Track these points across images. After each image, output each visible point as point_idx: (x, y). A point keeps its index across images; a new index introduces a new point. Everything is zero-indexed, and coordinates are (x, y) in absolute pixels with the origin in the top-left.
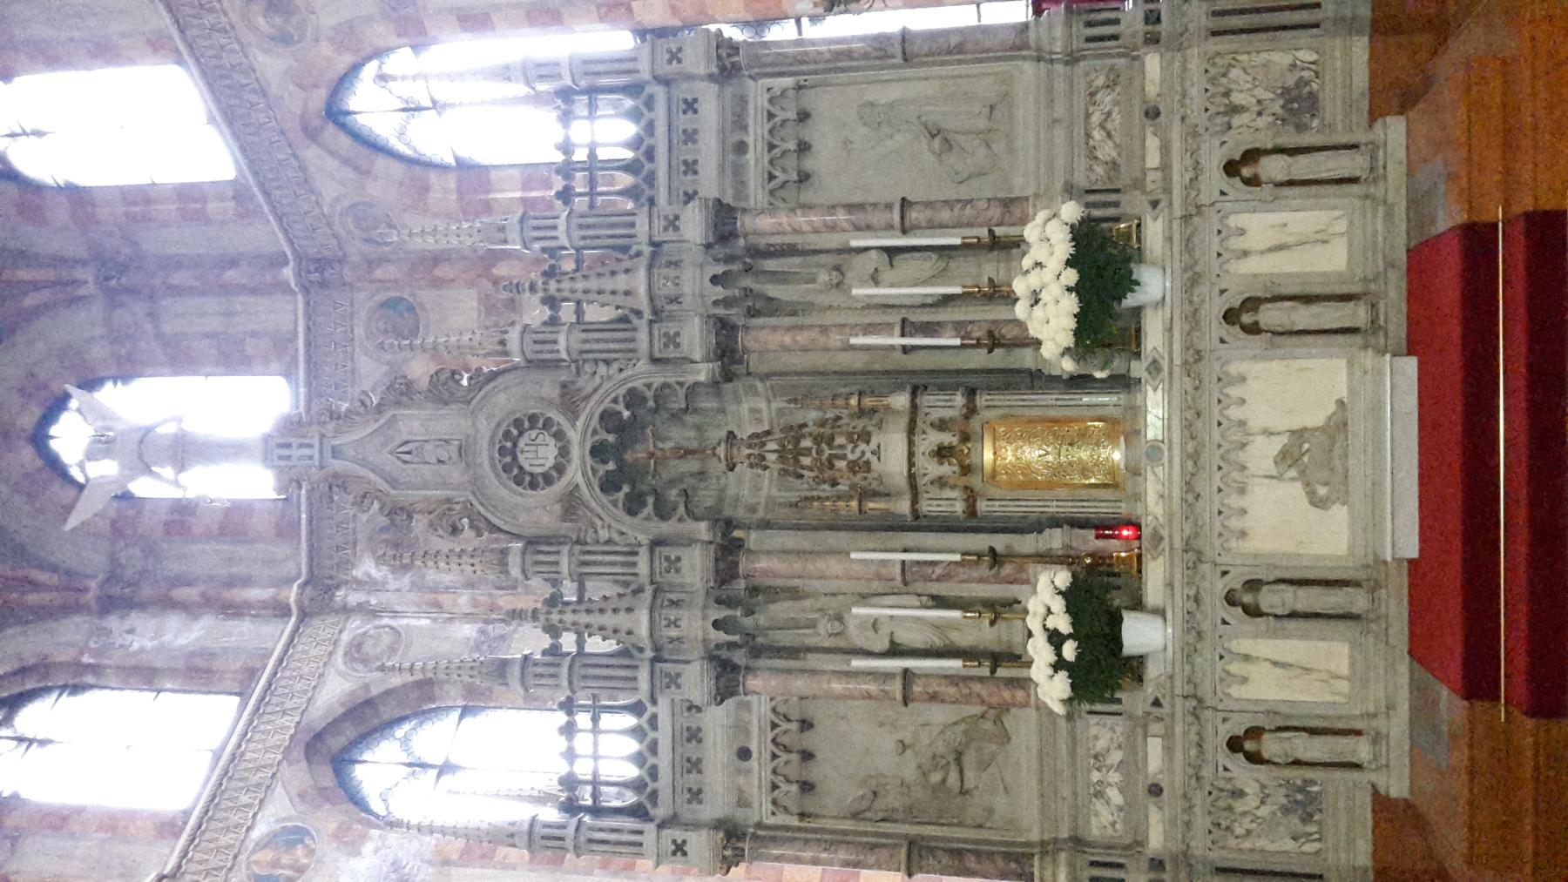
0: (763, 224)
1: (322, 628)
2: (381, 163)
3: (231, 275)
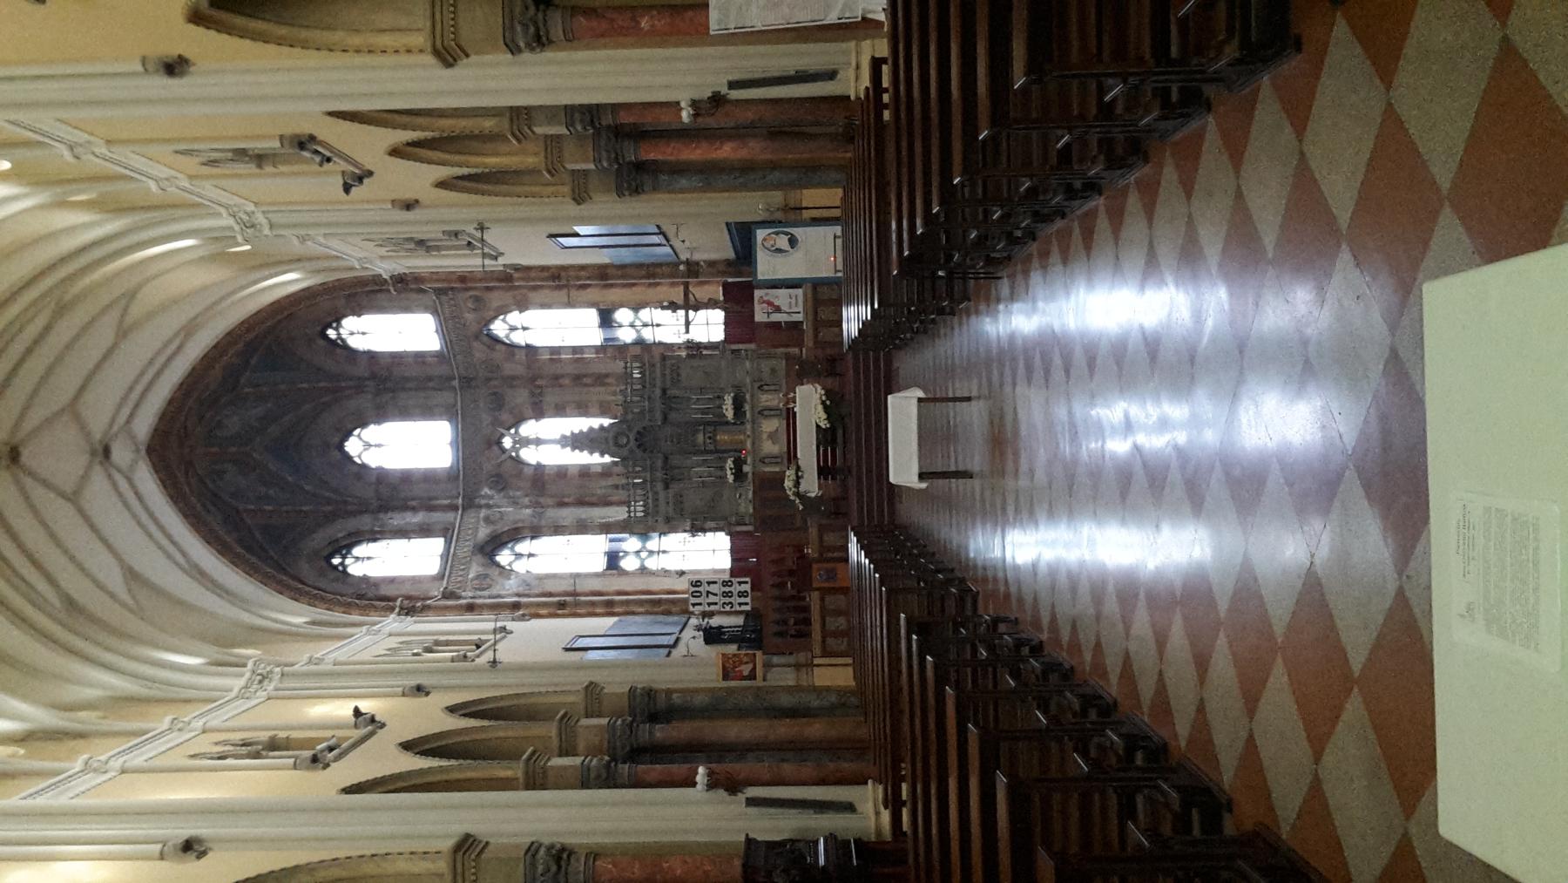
0: (673, 392)
1: (472, 513)
2: (498, 347)
3: (431, 384)
